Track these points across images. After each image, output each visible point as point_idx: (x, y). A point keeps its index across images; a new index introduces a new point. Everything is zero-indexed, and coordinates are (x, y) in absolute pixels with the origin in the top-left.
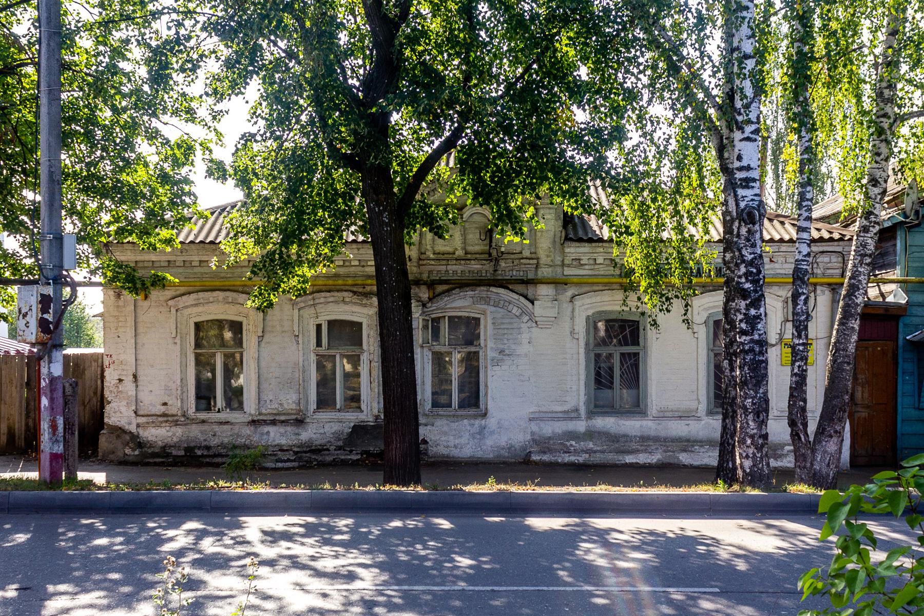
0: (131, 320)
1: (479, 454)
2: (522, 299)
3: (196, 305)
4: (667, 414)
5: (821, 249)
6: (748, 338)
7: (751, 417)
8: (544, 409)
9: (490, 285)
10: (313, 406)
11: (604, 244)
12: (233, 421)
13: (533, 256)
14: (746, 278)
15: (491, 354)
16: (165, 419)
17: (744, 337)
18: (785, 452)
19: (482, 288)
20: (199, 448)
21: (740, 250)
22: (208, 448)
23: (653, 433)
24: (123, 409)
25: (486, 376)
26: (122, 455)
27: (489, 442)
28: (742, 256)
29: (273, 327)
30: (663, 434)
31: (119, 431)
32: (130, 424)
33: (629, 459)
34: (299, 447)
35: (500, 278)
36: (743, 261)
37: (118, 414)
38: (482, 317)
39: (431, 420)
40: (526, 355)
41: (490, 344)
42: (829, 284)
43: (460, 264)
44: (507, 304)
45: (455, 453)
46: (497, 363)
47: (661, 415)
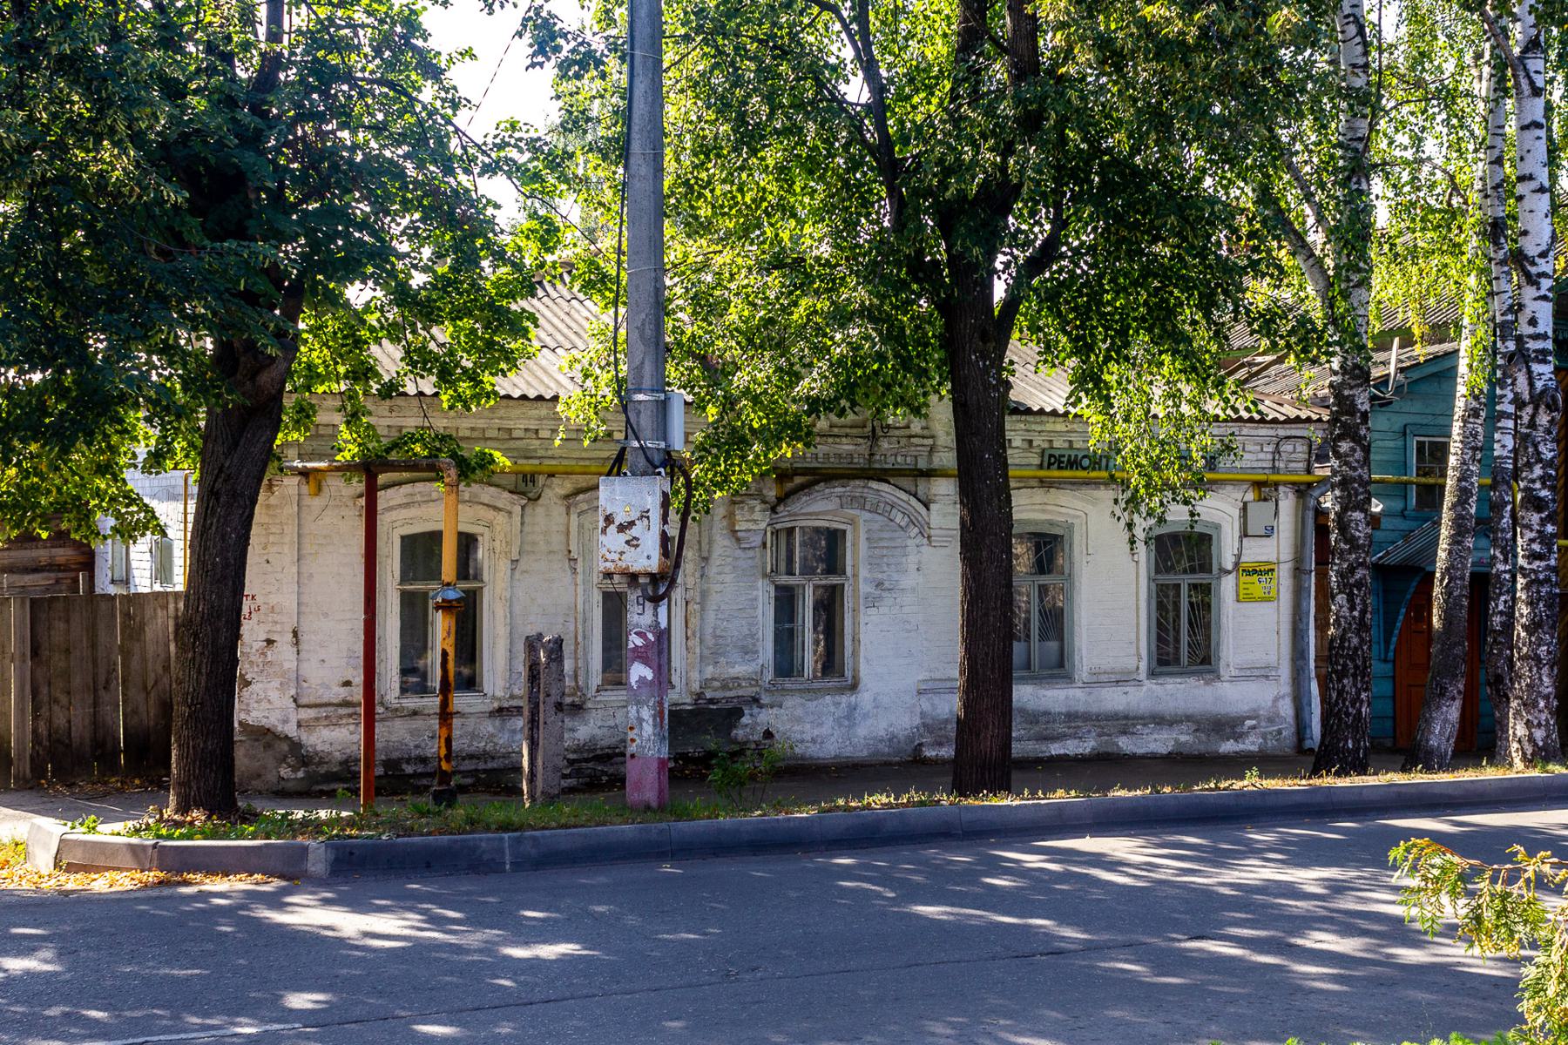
0: (291, 530)
1: (848, 752)
2: (913, 501)
3: (407, 505)
4: (1104, 678)
5: (1289, 433)
6: (1543, 564)
7: (1545, 670)
8: (937, 675)
9: (869, 478)
10: (596, 679)
11: (1030, 418)
12: (468, 710)
13: (926, 432)
14: (1543, 484)
15: (865, 588)
16: (351, 710)
17: (1537, 563)
18: (1245, 729)
19: (857, 482)
20: (408, 761)
21: (1536, 446)
22: (423, 760)
23: (1081, 708)
24: (274, 695)
25: (855, 624)
26: (275, 780)
27: (862, 731)
28: (1539, 453)
29: (534, 543)
30: (1094, 709)
31: (264, 736)
32: (286, 721)
33: (1056, 749)
34: (575, 752)
35: (877, 466)
36: (1540, 460)
37: (265, 705)
38: (849, 528)
39: (778, 698)
40: (913, 589)
41: (863, 573)
42: (1294, 483)
43: (826, 443)
44: (888, 508)
45: (813, 751)
46: (873, 602)
47: (1095, 679)
